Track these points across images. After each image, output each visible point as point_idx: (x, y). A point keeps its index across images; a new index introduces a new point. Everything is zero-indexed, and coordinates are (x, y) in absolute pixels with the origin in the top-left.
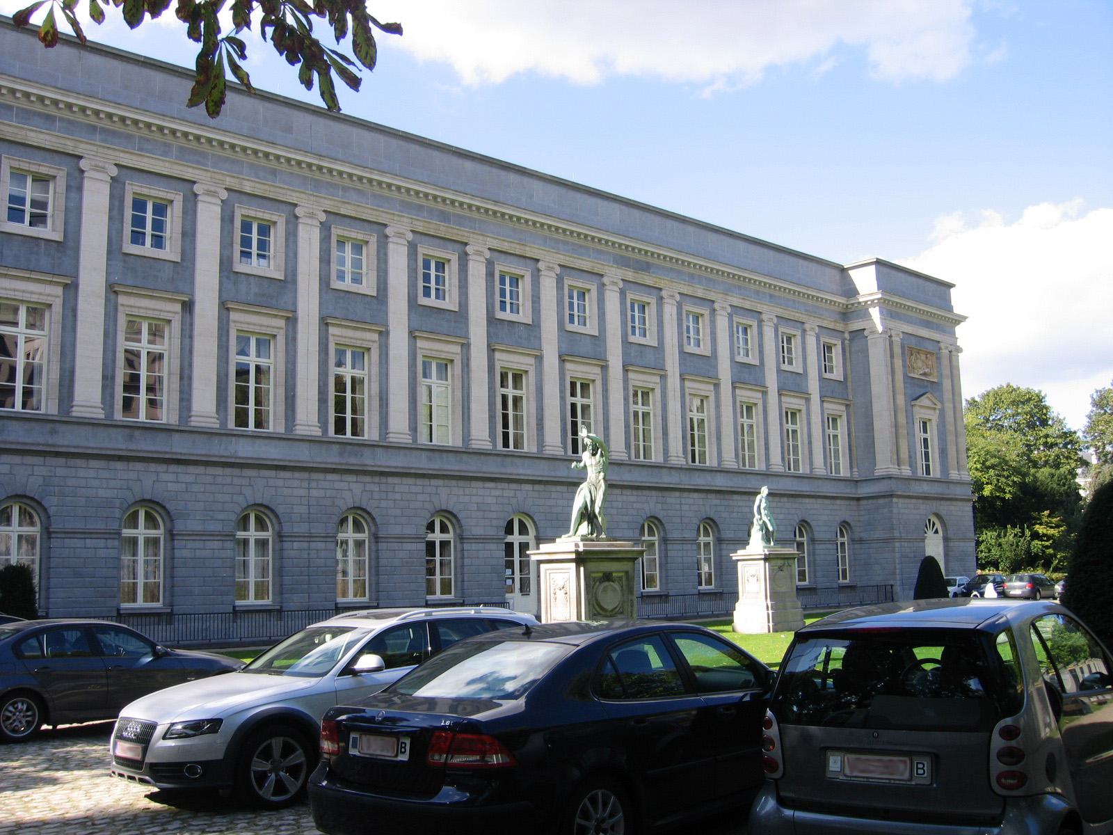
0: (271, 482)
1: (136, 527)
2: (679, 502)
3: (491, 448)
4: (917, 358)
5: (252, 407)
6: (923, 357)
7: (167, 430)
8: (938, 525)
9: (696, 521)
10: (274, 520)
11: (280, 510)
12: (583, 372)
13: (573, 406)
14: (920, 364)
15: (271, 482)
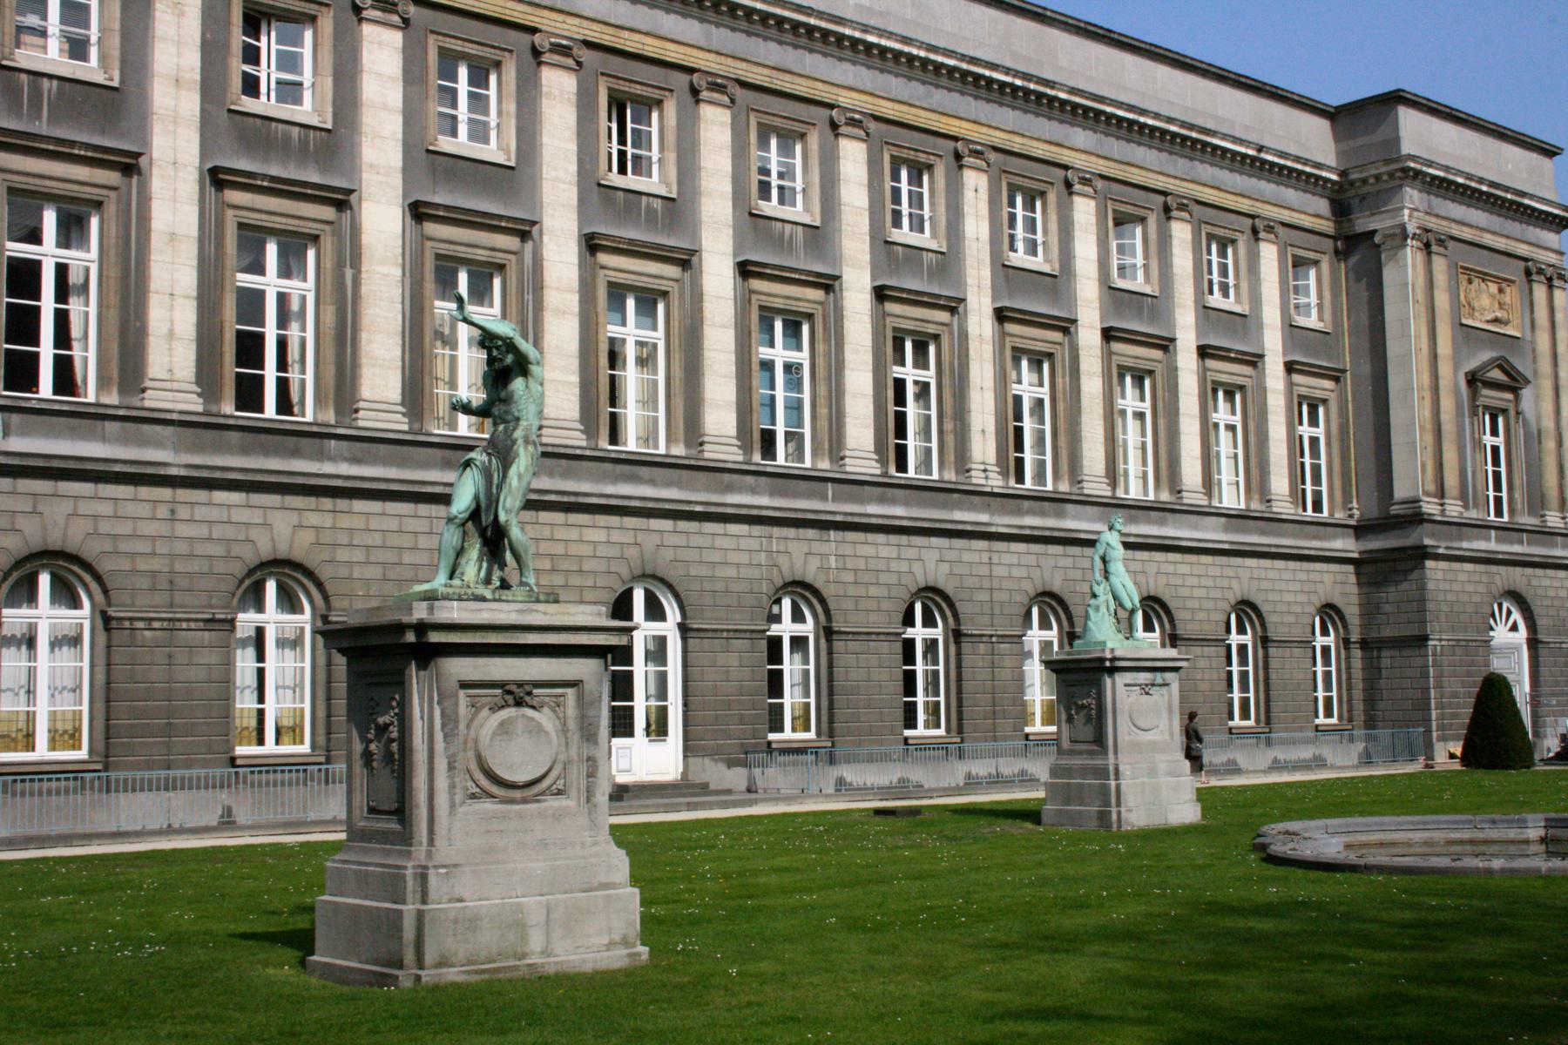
0: (85, 508)
1: (260, 608)
2: (985, 560)
4: (1479, 291)
5: (47, 351)
6: (1493, 288)
7: (316, 435)
8: (1516, 616)
9: (1021, 598)
10: (94, 586)
11: (1173, 604)
14: (1485, 302)
15: (85, 508)
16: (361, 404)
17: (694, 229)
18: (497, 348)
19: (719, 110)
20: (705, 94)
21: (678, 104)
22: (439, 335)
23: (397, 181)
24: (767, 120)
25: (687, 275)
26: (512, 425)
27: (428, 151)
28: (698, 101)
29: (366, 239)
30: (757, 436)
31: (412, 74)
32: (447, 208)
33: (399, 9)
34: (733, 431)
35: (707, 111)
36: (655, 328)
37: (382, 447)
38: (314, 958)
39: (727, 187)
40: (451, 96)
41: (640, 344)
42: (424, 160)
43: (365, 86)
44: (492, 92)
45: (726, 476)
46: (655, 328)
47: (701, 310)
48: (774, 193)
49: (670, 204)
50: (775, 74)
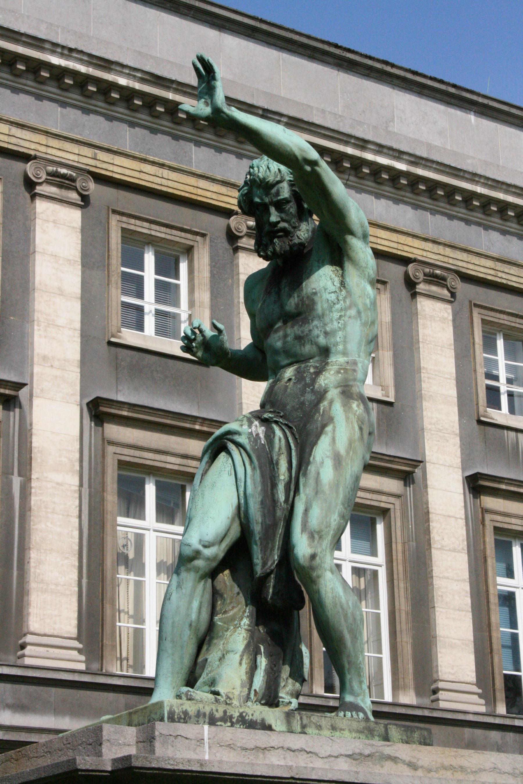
16: (29, 638)
17: (417, 437)
18: (280, 205)
19: (439, 306)
20: (422, 287)
21: (392, 298)
22: (123, 559)
23: (74, 375)
24: (491, 317)
25: (410, 490)
26: (312, 365)
27: (110, 343)
28: (414, 295)
29: (38, 441)
30: (499, 683)
31: (92, 258)
32: (132, 406)
33: (78, 184)
34: (471, 675)
35: (424, 305)
36: (374, 553)
37: (54, 691)
38: (206, 727)
39: (451, 391)
40: (136, 286)
41: (357, 572)
42: (104, 351)
43: (38, 269)
44: (183, 281)
45: (467, 732)
46: (374, 553)
47: (428, 531)
48: (504, 400)
49: (387, 409)
50: (499, 266)
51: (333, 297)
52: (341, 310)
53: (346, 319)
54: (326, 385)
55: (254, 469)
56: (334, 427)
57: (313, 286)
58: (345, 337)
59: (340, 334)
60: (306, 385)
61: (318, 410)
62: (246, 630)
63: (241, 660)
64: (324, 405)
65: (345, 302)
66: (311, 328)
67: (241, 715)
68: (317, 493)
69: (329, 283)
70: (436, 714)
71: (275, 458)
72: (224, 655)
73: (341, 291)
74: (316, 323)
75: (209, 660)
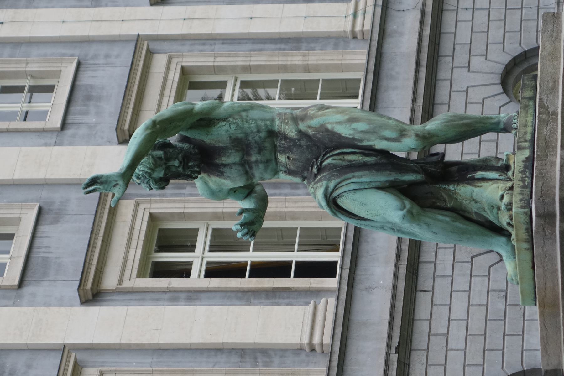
3: (332, 301)
12: (128, 247)
13: (214, 271)
51: (233, 126)
52: (242, 121)
53: (249, 118)
54: (296, 131)
55: (354, 177)
56: (328, 123)
57: (225, 139)
58: (261, 119)
59: (259, 123)
60: (295, 145)
61: (315, 136)
62: (457, 186)
63: (478, 186)
64: (310, 132)
65: (237, 119)
66: (254, 141)
67: (521, 172)
68: (375, 132)
69: (223, 128)
70: (337, 348)
71: (346, 163)
72: (473, 200)
73: (229, 121)
74: (250, 138)
75: (476, 210)
